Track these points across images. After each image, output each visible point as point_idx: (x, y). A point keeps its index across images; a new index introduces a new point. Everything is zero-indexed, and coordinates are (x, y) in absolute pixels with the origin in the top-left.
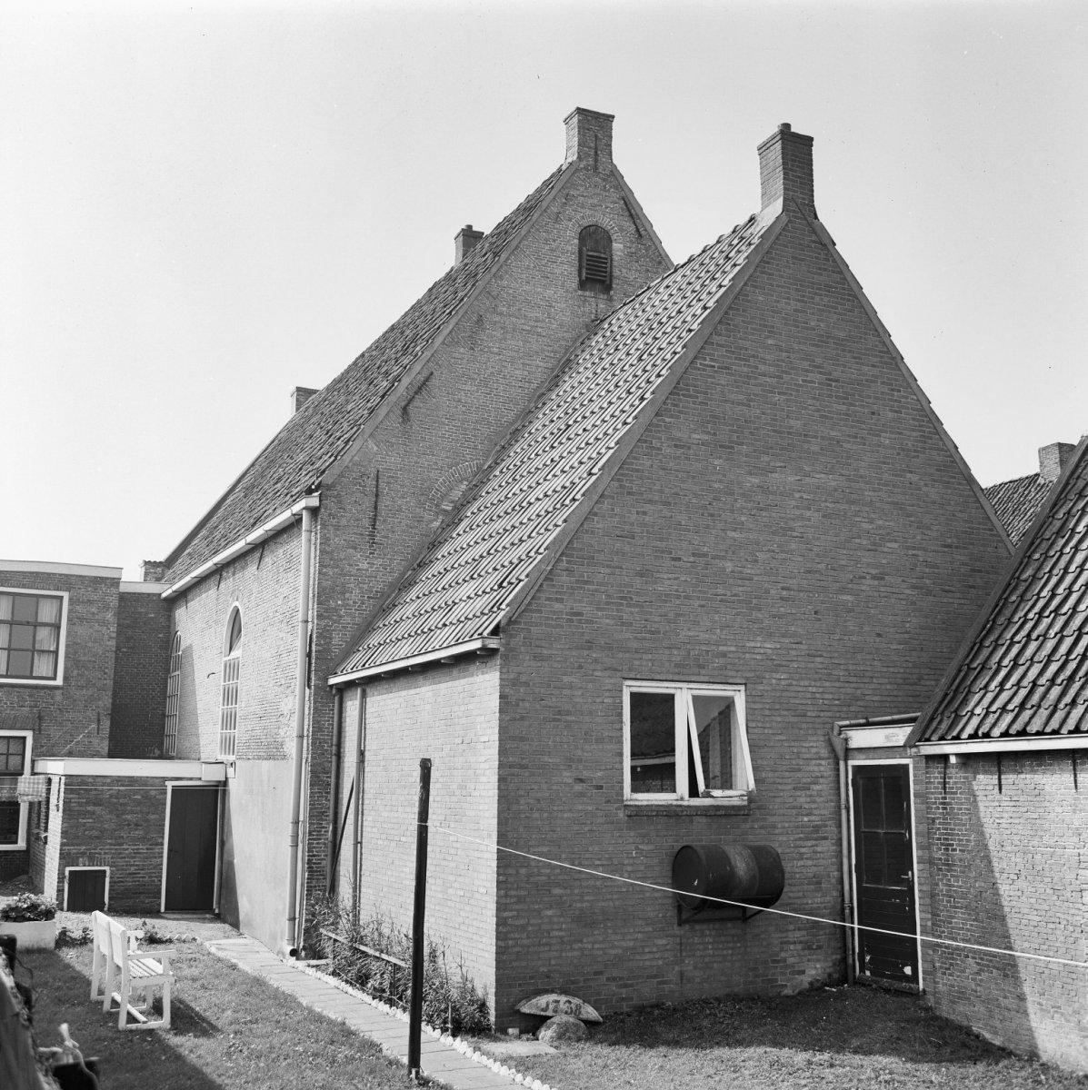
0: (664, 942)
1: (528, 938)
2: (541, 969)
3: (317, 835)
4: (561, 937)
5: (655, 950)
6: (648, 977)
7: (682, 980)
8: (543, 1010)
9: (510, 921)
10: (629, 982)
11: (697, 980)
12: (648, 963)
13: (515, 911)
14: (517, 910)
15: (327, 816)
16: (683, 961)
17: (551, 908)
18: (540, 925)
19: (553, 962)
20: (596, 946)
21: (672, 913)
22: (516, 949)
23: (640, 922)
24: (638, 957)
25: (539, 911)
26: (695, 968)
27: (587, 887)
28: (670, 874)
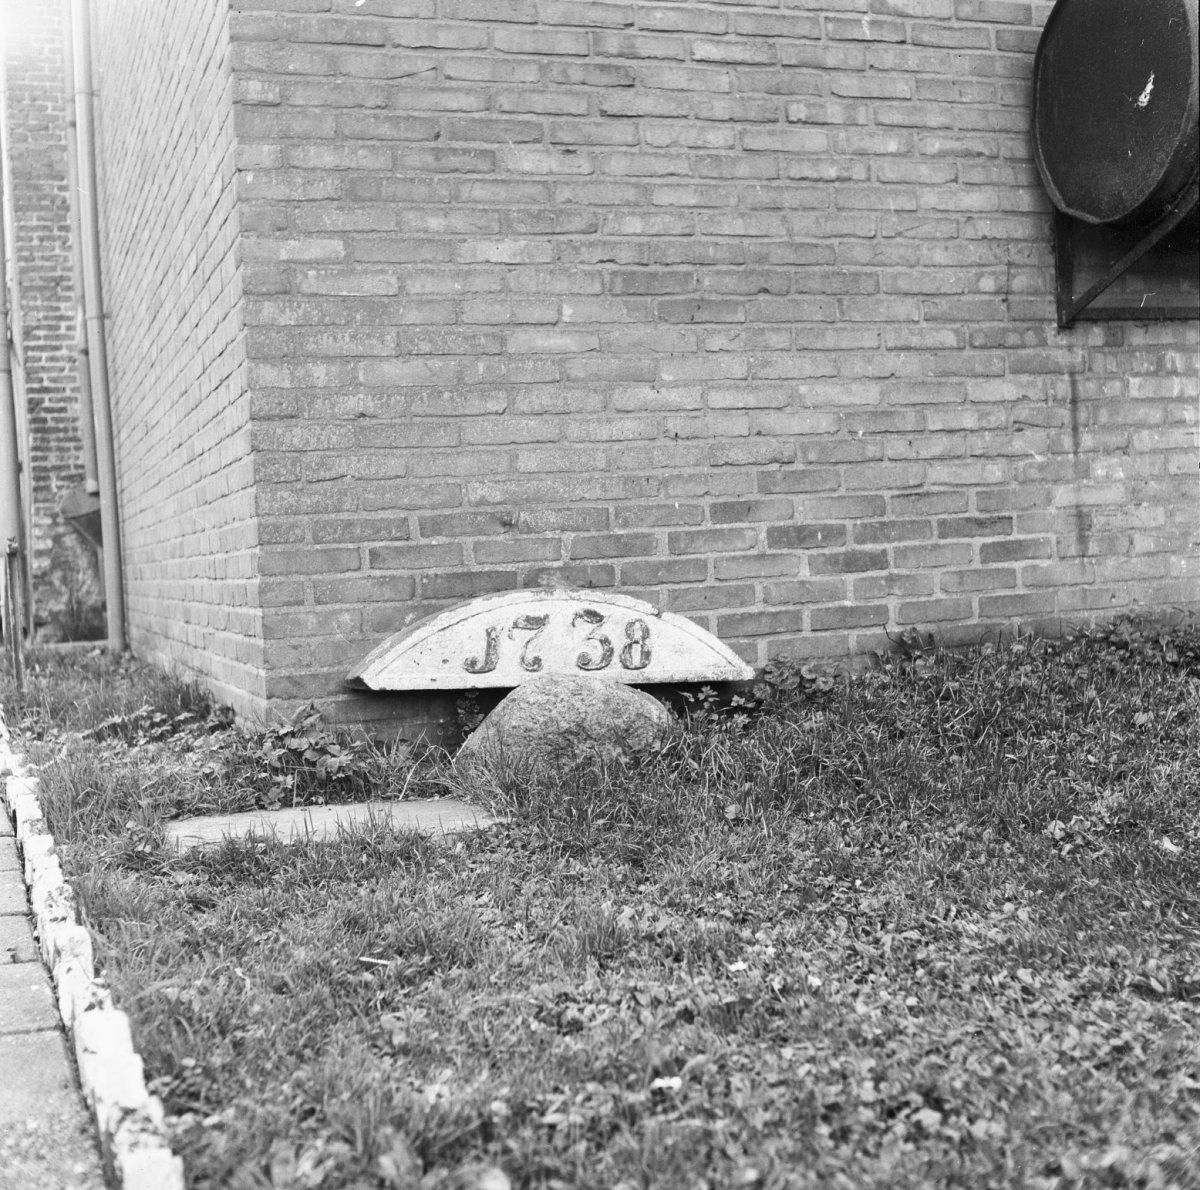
0: (1007, 390)
1: (403, 354)
2: (477, 492)
3: (46, 337)
4: (562, 358)
5: (969, 421)
6: (945, 530)
7: (1082, 540)
8: (471, 666)
9: (310, 282)
10: (869, 547)
11: (1143, 543)
12: (940, 473)
13: (332, 234)
14: (342, 234)
15: (69, 288)
16: (1082, 471)
17: (505, 228)
18: (457, 302)
19: (528, 461)
20: (718, 399)
21: (1033, 279)
22: (354, 403)
23: (904, 308)
24: (897, 446)
25: (449, 243)
26: (1136, 497)
27: (664, 151)
28: (1020, 122)
